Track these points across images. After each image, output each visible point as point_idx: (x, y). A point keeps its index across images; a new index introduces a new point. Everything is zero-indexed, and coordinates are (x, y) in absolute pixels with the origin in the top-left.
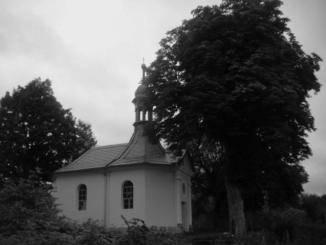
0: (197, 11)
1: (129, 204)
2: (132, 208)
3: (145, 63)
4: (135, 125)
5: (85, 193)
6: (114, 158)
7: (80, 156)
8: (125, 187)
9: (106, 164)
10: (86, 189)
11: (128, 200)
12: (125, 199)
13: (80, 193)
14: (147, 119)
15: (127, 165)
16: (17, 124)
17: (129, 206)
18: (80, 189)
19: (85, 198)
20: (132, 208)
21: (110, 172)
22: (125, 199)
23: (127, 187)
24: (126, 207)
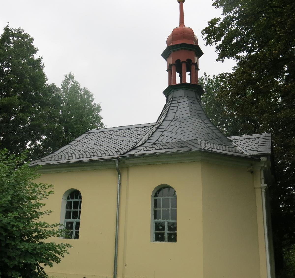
0: (43, 66)
1: (166, 231)
2: (174, 240)
3: (187, 24)
4: (167, 93)
5: (77, 205)
6: (133, 144)
7: (45, 156)
8: (70, 200)
9: (121, 153)
10: (80, 198)
11: (72, 223)
12: (68, 220)
13: (69, 205)
14: (188, 81)
15: (156, 155)
16: (261, 41)
17: (166, 236)
18: (68, 198)
19: (76, 215)
20: (174, 240)
21: (128, 168)
22: (68, 220)
23: (73, 200)
24: (159, 237)
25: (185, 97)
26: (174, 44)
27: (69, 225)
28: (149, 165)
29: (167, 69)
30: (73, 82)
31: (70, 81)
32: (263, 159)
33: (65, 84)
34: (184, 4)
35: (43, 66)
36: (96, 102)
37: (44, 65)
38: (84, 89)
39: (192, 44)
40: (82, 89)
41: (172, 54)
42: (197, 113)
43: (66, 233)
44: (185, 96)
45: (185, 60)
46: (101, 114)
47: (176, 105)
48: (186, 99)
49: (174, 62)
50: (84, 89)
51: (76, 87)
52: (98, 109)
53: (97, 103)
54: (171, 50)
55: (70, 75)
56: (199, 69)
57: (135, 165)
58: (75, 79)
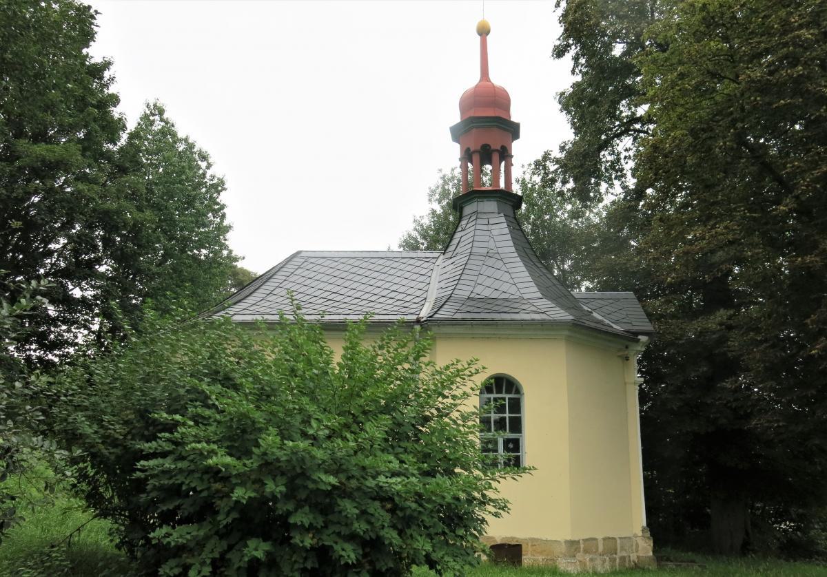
3: (497, 79)
25: (500, 215)
26: (477, 115)
27: (490, 446)
28: (473, 338)
29: (459, 157)
30: (162, 120)
31: (157, 118)
32: (643, 339)
33: (146, 120)
34: (489, 38)
35: (112, 80)
36: (218, 169)
37: (114, 77)
38: (186, 140)
39: (504, 117)
40: (181, 140)
41: (474, 130)
42: (523, 248)
43: (507, 461)
44: (499, 213)
45: (499, 148)
46: (223, 198)
47: (485, 227)
48: (503, 220)
49: (479, 148)
50: (186, 140)
51: (168, 131)
52: (219, 186)
53: (219, 175)
54: (473, 123)
55: (155, 105)
56: (512, 165)
57: (448, 337)
58: (165, 116)
